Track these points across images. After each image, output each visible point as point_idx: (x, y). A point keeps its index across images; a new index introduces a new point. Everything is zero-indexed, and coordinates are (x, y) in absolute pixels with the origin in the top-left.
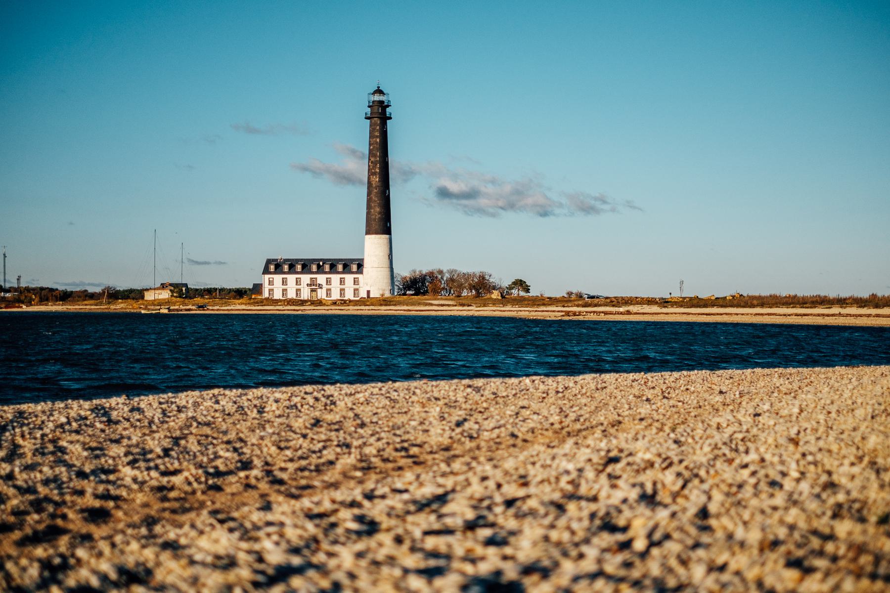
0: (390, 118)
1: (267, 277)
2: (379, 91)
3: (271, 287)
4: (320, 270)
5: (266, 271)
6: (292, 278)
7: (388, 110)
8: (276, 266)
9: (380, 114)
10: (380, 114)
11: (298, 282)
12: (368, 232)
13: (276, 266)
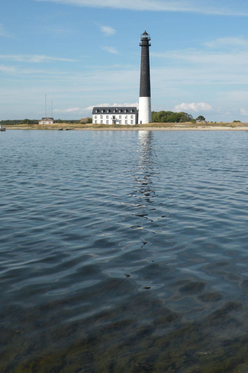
0: (150, 45)
1: (94, 115)
2: (146, 34)
3: (96, 119)
4: (117, 112)
5: (94, 113)
6: (104, 116)
7: (149, 42)
8: (98, 111)
9: (146, 44)
10: (146, 44)
11: (107, 117)
12: (141, 96)
13: (98, 111)
